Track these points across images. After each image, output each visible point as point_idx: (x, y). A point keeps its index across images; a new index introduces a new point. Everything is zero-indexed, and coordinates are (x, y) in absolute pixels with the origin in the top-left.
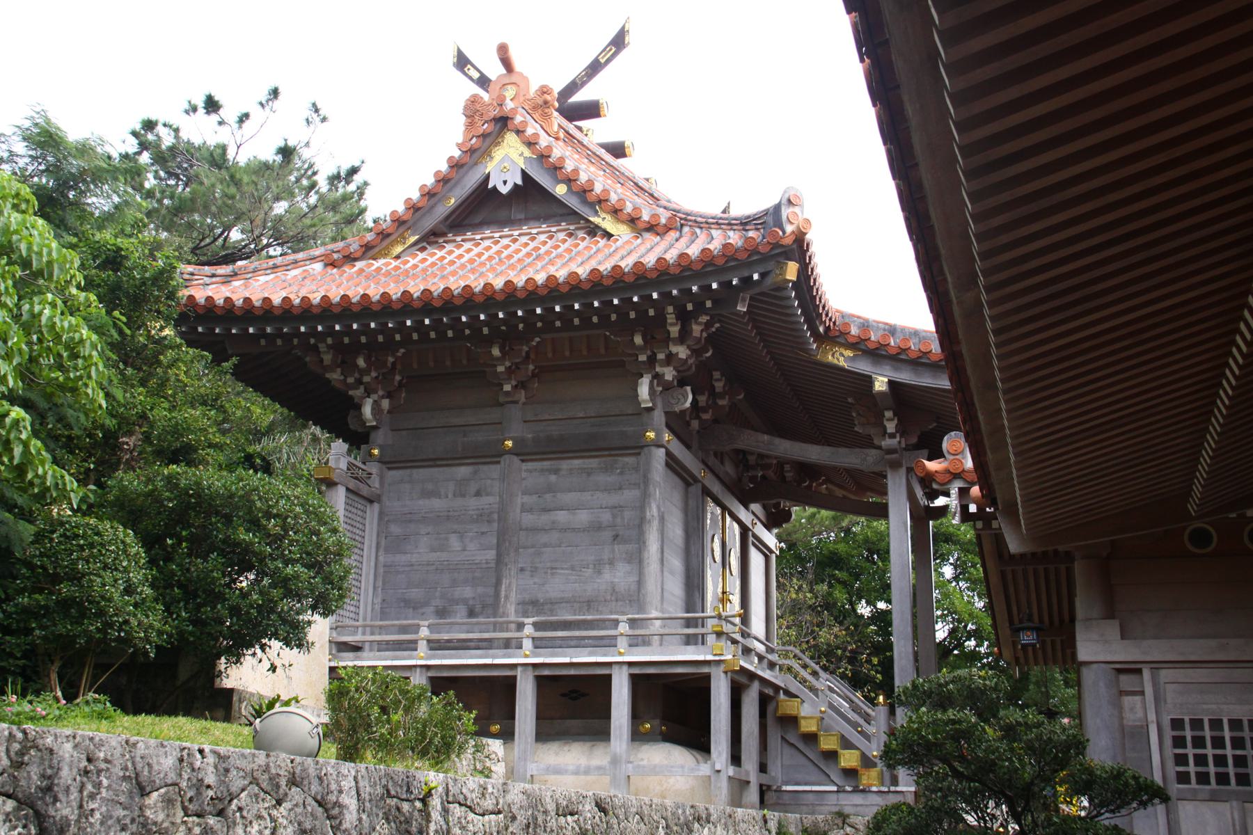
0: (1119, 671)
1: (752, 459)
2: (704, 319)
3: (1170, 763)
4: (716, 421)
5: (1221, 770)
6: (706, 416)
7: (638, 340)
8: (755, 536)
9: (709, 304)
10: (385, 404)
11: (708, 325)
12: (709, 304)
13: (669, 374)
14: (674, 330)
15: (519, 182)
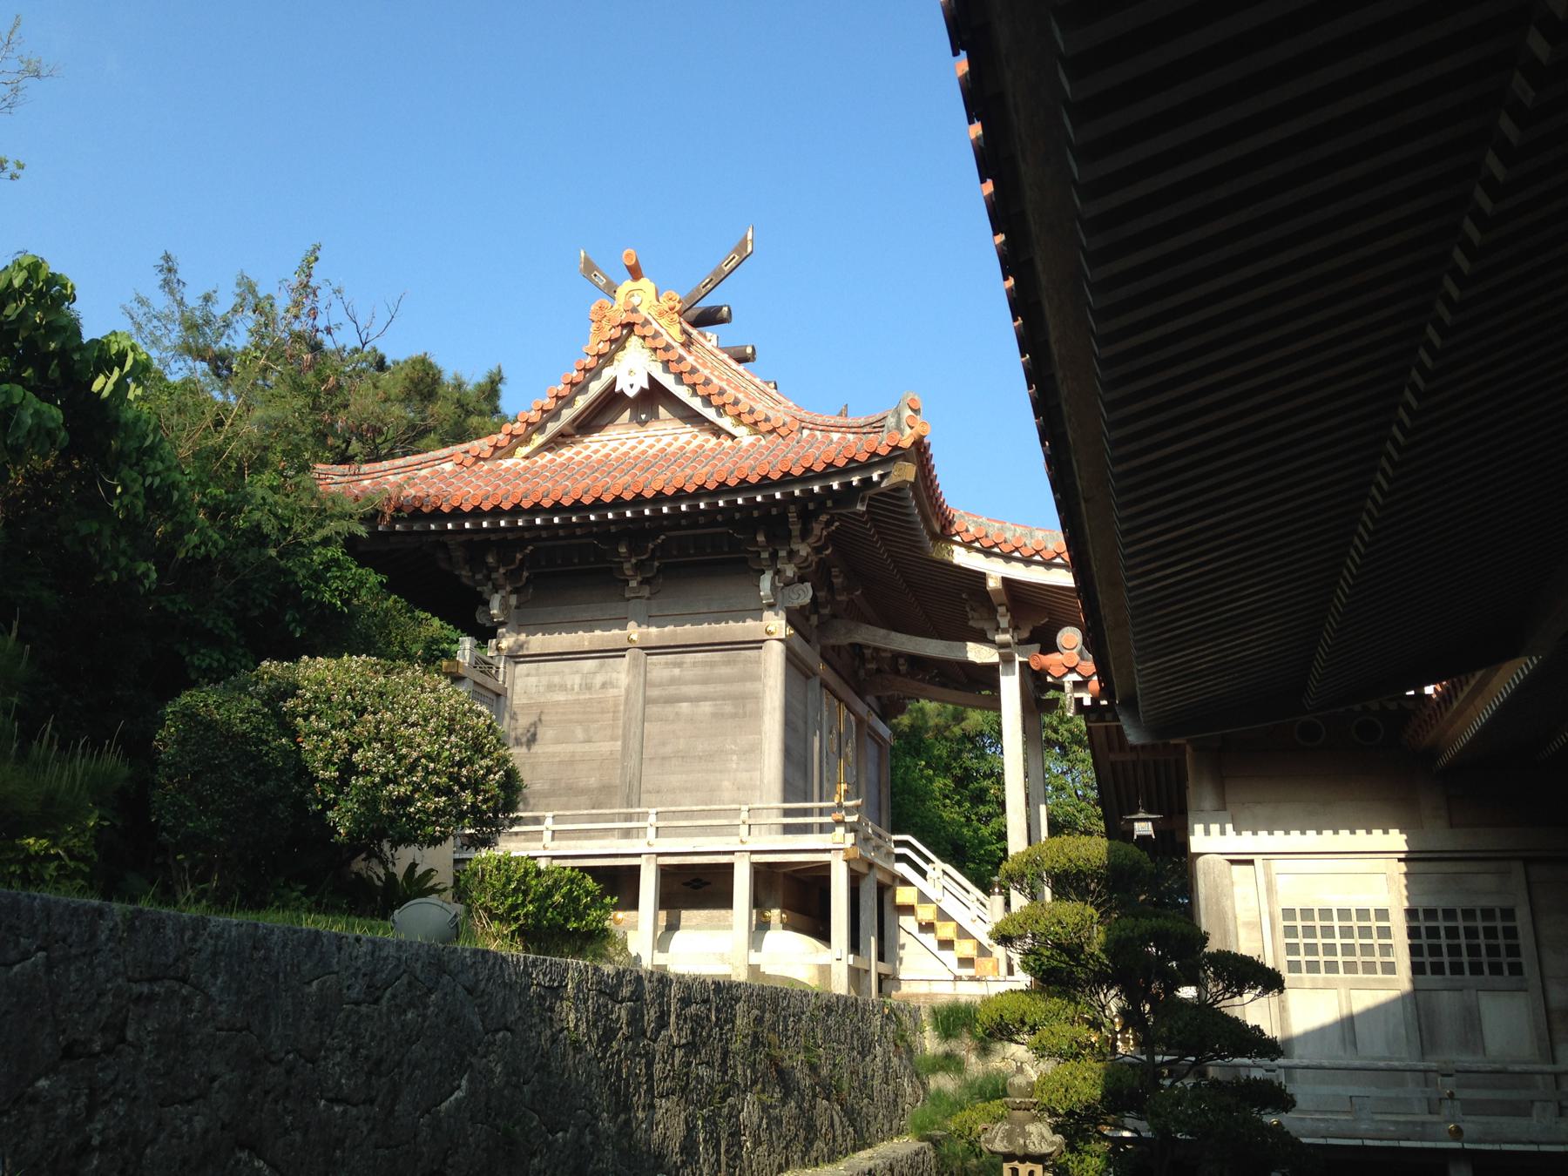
0: (1233, 862)
1: (868, 652)
2: (824, 518)
3: (1282, 951)
4: (834, 616)
5: (1455, 959)
6: (826, 611)
7: (761, 538)
8: (870, 727)
9: (829, 503)
10: (513, 600)
11: (828, 524)
12: (829, 503)
13: (790, 571)
14: (796, 529)
15: (646, 386)
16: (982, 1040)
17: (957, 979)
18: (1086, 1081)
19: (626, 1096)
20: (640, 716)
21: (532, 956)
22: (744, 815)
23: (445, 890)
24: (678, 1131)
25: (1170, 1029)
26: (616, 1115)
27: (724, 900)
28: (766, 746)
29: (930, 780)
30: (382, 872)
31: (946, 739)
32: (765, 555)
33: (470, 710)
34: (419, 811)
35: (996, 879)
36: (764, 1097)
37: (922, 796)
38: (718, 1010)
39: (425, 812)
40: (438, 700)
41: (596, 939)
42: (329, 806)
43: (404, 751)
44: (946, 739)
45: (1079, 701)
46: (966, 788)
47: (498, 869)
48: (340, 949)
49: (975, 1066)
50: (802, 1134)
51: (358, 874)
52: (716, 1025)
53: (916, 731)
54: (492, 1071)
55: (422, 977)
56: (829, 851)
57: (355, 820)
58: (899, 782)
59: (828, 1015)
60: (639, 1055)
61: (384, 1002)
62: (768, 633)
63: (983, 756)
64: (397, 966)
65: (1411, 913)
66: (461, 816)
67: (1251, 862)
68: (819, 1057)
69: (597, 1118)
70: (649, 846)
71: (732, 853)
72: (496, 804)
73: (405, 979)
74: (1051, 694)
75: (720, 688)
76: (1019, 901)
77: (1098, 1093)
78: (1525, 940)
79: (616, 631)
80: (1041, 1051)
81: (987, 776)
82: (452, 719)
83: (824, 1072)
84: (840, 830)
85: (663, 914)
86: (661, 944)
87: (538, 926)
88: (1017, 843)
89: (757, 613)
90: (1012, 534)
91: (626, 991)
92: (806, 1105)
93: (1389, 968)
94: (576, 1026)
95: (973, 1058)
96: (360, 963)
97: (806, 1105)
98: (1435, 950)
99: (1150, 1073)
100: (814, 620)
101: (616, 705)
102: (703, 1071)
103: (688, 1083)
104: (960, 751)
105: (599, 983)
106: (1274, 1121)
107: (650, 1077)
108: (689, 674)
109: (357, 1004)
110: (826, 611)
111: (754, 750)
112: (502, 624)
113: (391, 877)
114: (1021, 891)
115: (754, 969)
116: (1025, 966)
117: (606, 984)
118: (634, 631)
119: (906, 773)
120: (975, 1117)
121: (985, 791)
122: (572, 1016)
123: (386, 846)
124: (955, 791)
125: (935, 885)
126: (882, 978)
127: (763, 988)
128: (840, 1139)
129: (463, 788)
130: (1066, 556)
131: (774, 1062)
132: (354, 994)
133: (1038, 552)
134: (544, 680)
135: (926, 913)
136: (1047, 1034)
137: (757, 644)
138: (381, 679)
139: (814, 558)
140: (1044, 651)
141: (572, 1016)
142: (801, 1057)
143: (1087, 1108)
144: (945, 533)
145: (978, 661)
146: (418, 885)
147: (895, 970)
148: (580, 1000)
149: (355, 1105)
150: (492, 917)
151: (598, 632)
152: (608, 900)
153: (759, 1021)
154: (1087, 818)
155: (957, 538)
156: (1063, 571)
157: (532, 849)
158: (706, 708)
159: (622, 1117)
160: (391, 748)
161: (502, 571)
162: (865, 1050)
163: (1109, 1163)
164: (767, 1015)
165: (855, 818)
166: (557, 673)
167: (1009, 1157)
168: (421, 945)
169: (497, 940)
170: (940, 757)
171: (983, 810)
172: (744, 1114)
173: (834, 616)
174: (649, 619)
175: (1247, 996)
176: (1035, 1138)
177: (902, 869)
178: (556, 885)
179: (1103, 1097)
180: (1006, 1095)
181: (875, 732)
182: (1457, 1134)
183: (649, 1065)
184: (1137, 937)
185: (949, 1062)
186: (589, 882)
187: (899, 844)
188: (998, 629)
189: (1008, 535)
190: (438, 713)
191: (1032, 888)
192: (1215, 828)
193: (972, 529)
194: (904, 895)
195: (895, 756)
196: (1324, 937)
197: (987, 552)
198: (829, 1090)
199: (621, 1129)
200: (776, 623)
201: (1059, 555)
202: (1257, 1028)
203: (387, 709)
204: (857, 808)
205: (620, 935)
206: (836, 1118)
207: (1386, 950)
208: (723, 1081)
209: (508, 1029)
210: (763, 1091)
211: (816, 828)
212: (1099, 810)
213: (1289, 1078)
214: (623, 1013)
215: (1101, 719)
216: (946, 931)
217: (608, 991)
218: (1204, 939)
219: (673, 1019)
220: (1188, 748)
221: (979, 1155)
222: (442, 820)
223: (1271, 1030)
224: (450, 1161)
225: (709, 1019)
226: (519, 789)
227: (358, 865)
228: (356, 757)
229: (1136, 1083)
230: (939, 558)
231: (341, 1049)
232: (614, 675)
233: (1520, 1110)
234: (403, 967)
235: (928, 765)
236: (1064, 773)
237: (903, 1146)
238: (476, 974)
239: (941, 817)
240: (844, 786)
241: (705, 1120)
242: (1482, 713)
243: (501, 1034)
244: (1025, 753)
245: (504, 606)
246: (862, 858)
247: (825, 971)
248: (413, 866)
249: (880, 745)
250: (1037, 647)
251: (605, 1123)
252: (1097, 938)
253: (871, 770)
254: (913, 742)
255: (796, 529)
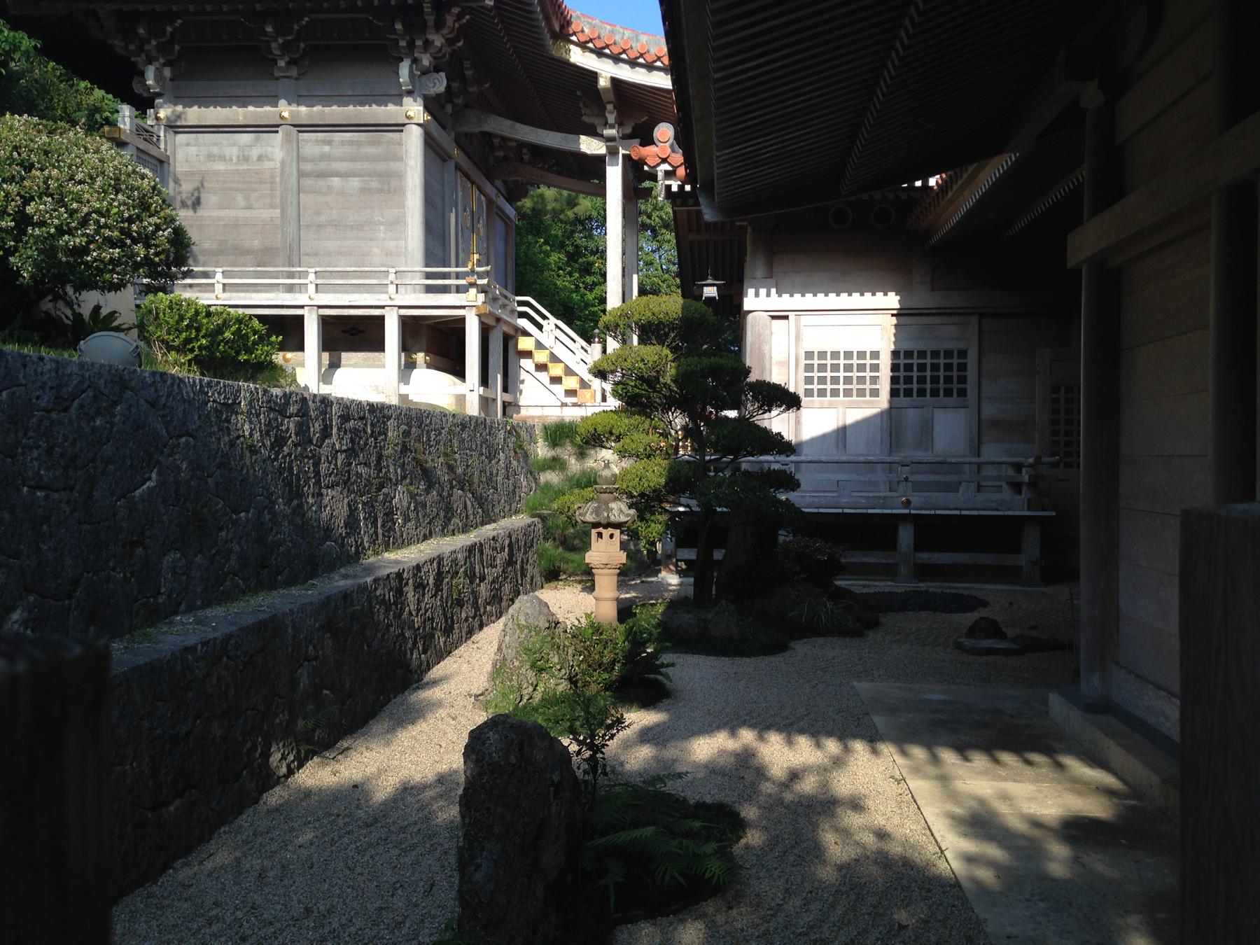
1: (496, 141)
4: (466, 106)
6: (459, 101)
7: (398, 26)
10: (167, 72)
11: (460, 16)
13: (426, 61)
14: (430, 19)
16: (580, 447)
17: (564, 405)
18: (655, 474)
19: (298, 486)
20: (295, 188)
21: (206, 379)
22: (392, 277)
23: (130, 329)
24: (342, 511)
25: (718, 437)
26: (290, 501)
27: (378, 345)
28: (409, 220)
29: (548, 255)
30: (69, 312)
31: (561, 221)
32: (403, 43)
33: (134, 172)
34: (95, 260)
35: (597, 331)
36: (412, 488)
37: (541, 268)
38: (372, 425)
39: (102, 261)
40: (102, 160)
41: (265, 370)
42: (11, 252)
43: (75, 205)
44: (561, 221)
45: (668, 187)
46: (576, 262)
47: (171, 308)
48: (24, 366)
49: (574, 465)
50: (442, 514)
51: (46, 313)
52: (372, 436)
53: (537, 213)
54: (179, 468)
55: (106, 392)
56: (464, 307)
57: (36, 265)
58: (522, 255)
59: (463, 430)
60: (307, 457)
61: (72, 410)
62: (408, 117)
63: (590, 237)
64: (81, 382)
65: (895, 354)
66: (137, 266)
67: (786, 317)
68: (456, 461)
69: (274, 503)
70: (311, 299)
71: (383, 307)
72: (167, 257)
73: (90, 393)
74: (647, 184)
75: (367, 166)
76: (613, 345)
77: (663, 481)
78: (971, 373)
79: (268, 108)
80: (622, 454)
81: (594, 253)
82: (117, 179)
83: (459, 471)
84: (473, 291)
85: (326, 355)
86: (326, 378)
87: (212, 357)
88: (614, 300)
89: (397, 98)
90: (620, 37)
91: (293, 409)
92: (445, 494)
93: (875, 393)
94: (251, 435)
95: (573, 461)
96: (45, 378)
97: (445, 494)
98: (908, 380)
99: (700, 468)
100: (449, 108)
101: (273, 177)
102: (360, 469)
103: (349, 478)
104: (573, 232)
105: (268, 402)
106: (784, 498)
107: (317, 473)
108: (338, 151)
109: (48, 411)
110: (459, 101)
111: (398, 223)
112: (159, 95)
113: (78, 317)
114: (615, 338)
115: (404, 398)
116: (615, 394)
117: (275, 403)
118: (285, 110)
119: (528, 248)
120: (573, 499)
121: (591, 264)
122: (247, 427)
123: (70, 290)
124: (567, 264)
125: (549, 336)
126: (505, 405)
127: (410, 410)
128: (471, 517)
129: (135, 241)
130: (666, 60)
131: (420, 464)
132: (43, 403)
133: (642, 55)
134: (204, 151)
135: (541, 357)
136: (628, 441)
137: (399, 127)
138: (45, 138)
139: (447, 49)
140: (643, 144)
141: (247, 427)
142: (441, 460)
143: (654, 491)
144: (563, 34)
145: (589, 152)
146: (101, 321)
147: (516, 400)
148: (252, 414)
149: (57, 491)
150: (170, 348)
151: (251, 108)
152: (273, 338)
153: (407, 434)
154: (669, 286)
155: (574, 38)
156: (662, 74)
157: (205, 299)
158: (355, 183)
159: (295, 502)
160: (61, 202)
161: (154, 42)
162: (492, 455)
163: (668, 527)
164: (413, 430)
165: (485, 281)
166: (216, 144)
167: (596, 525)
168: (102, 366)
169: (176, 366)
170: (556, 236)
171: (589, 279)
172: (396, 500)
173: (466, 106)
174: (298, 99)
175: (775, 412)
176: (615, 512)
177: (523, 323)
178: (226, 324)
179: (667, 483)
180: (596, 483)
181: (504, 213)
182: (907, 504)
183: (317, 464)
184: (702, 370)
185: (555, 463)
186: (256, 323)
187: (521, 303)
188: (606, 125)
189: (618, 38)
190: (103, 173)
191: (623, 335)
192: (763, 291)
193: (586, 30)
194: (524, 344)
195: (519, 234)
196: (830, 371)
197: (599, 53)
198: (463, 483)
199: (294, 510)
200: (414, 109)
201: (659, 59)
202: (779, 434)
203: (54, 167)
204: (487, 274)
205: (289, 370)
206: (469, 503)
207: (874, 380)
208: (378, 476)
209: (190, 435)
210: (411, 484)
211: (454, 289)
212: (678, 281)
213: (797, 469)
214: (292, 426)
215: (685, 204)
216: (557, 370)
217: (279, 408)
218: (748, 372)
219: (335, 431)
220: (749, 230)
221: (575, 525)
222: (118, 269)
223: (788, 435)
224: (147, 533)
225: (365, 432)
226: (188, 245)
227: (46, 305)
228: (30, 209)
229: (691, 474)
230: (558, 55)
231: (37, 447)
232: (269, 149)
233: (952, 488)
234: (87, 383)
235: (546, 243)
236: (653, 251)
237: (520, 521)
238: (156, 391)
239: (555, 284)
240: (476, 256)
241: (364, 504)
242: (968, 201)
243: (184, 439)
244: (624, 233)
245: (159, 77)
246: (491, 314)
247: (461, 399)
248: (97, 308)
249: (506, 224)
250: (637, 141)
251: (281, 505)
252: (671, 371)
253: (500, 245)
254: (534, 222)
255: (430, 19)
